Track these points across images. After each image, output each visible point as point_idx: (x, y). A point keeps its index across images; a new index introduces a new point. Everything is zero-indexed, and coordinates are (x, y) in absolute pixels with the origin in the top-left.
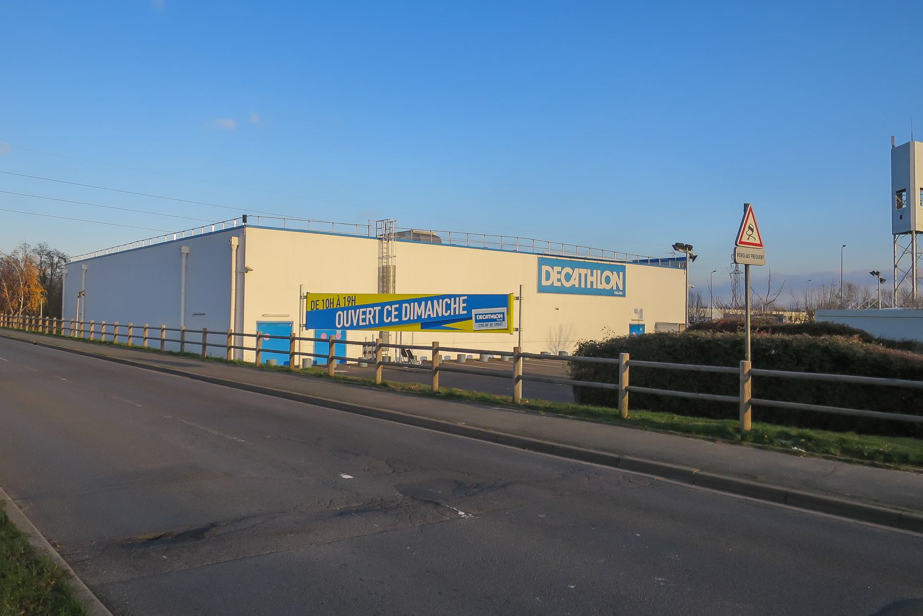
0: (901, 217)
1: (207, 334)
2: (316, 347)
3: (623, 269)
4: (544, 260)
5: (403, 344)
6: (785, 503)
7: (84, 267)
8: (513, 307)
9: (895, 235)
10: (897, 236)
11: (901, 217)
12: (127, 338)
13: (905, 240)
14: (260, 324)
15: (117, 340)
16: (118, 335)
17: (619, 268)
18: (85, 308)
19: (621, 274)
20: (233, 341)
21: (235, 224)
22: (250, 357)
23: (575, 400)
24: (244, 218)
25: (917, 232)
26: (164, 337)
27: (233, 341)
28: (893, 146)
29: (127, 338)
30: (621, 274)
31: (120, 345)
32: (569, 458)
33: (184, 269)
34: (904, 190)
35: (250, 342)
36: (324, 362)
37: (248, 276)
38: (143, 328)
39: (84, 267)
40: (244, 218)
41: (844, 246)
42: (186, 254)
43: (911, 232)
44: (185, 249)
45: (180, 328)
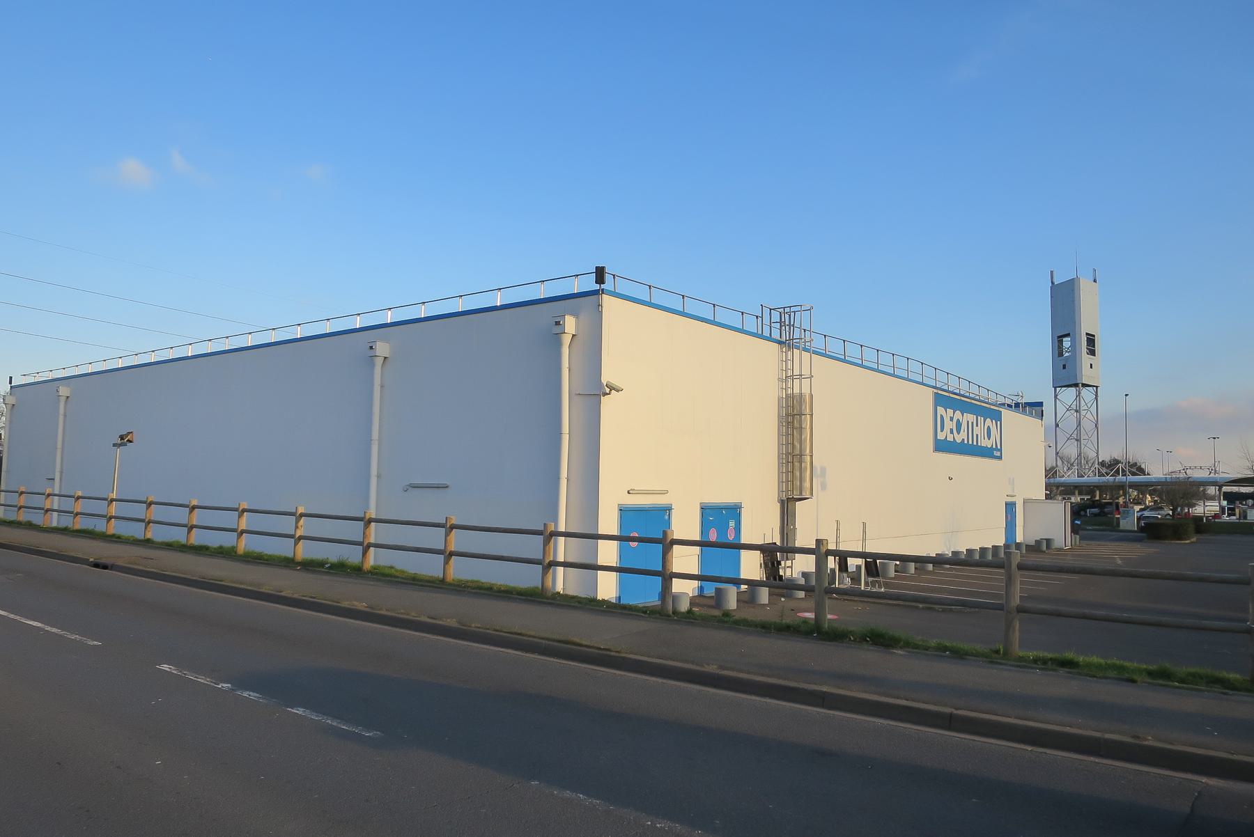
0: (1064, 367)
1: (674, 546)
2: (703, 560)
3: (997, 417)
4: (944, 399)
5: (842, 547)
6: (949, 728)
7: (64, 391)
8: (1198, 478)
9: (1055, 388)
10: (1058, 389)
11: (1064, 367)
12: (143, 525)
13: (1068, 395)
14: (625, 512)
15: (245, 544)
16: (377, 546)
17: (991, 413)
18: (62, 468)
19: (999, 422)
20: (562, 549)
21: (576, 287)
22: (607, 587)
23: (247, 550)
24: (600, 274)
25: (1085, 385)
26: (452, 548)
27: (562, 549)
28: (1052, 283)
29: (143, 525)
30: (999, 422)
31: (119, 537)
32: (363, 621)
33: (377, 388)
34: (1068, 335)
35: (608, 553)
36: (710, 589)
37: (608, 405)
38: (236, 510)
39: (64, 391)
40: (600, 274)
41: (1126, 395)
42: (65, 398)
43: (1076, 385)
44: (382, 349)
45: (188, 503)
